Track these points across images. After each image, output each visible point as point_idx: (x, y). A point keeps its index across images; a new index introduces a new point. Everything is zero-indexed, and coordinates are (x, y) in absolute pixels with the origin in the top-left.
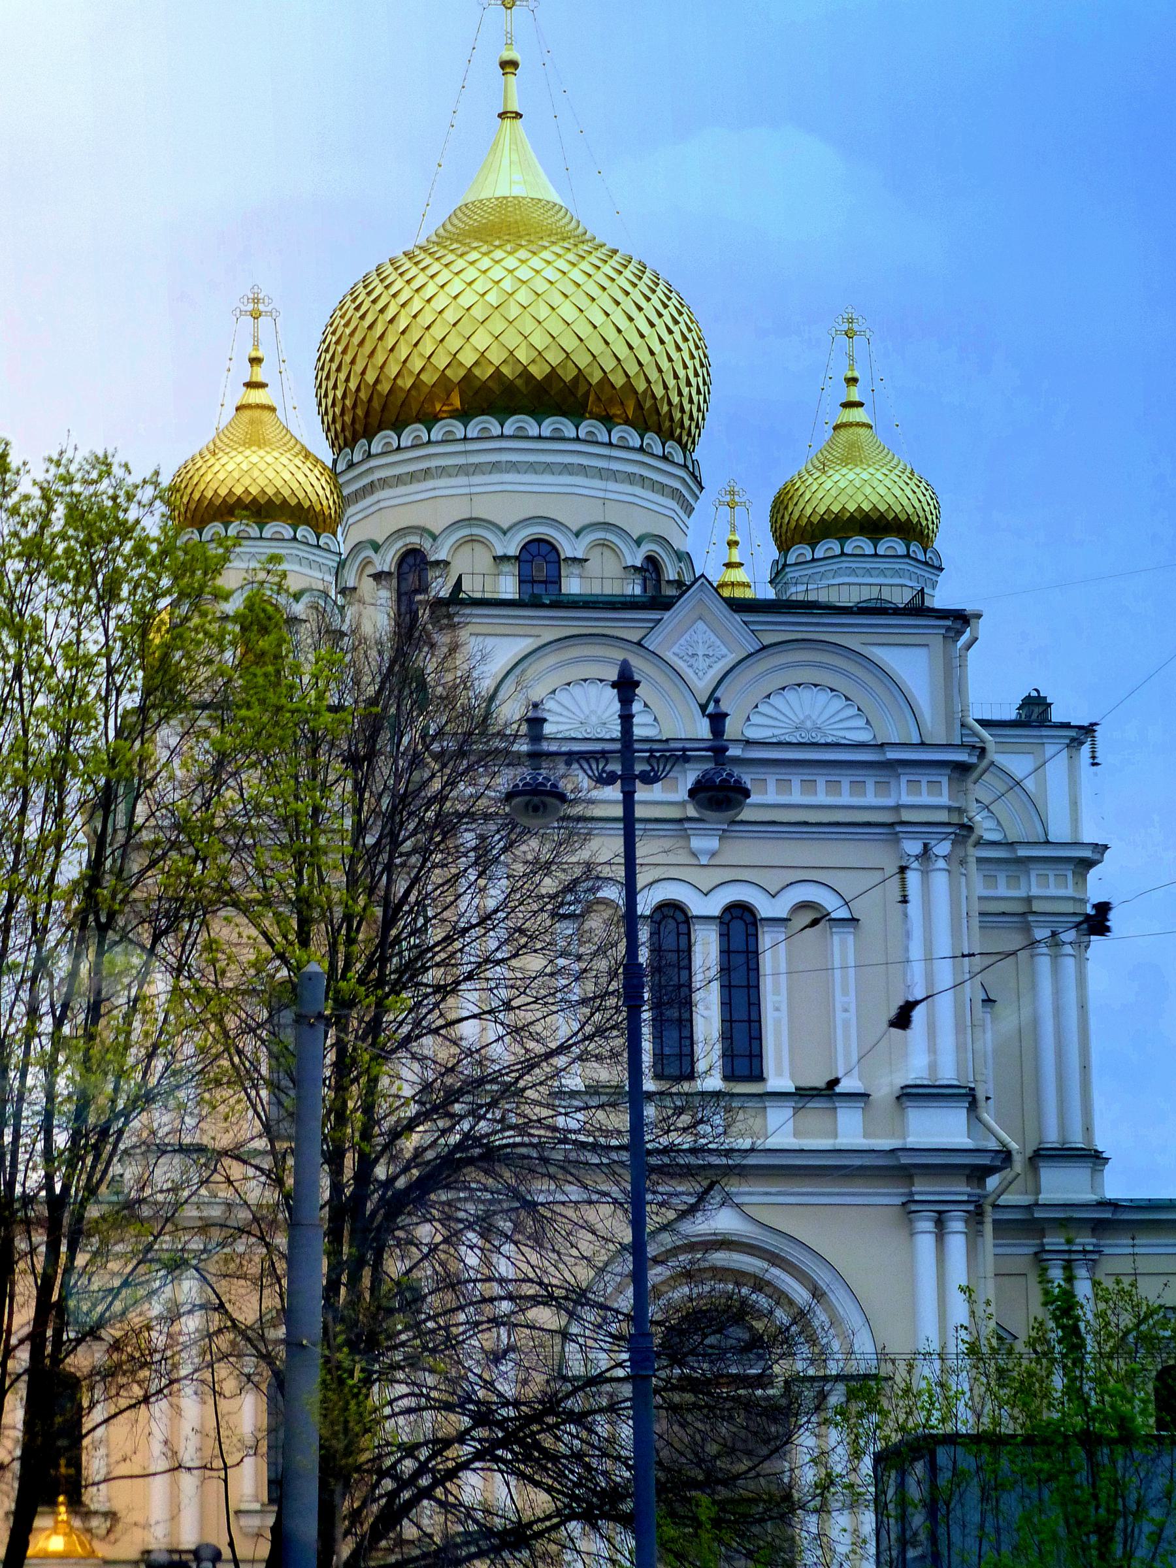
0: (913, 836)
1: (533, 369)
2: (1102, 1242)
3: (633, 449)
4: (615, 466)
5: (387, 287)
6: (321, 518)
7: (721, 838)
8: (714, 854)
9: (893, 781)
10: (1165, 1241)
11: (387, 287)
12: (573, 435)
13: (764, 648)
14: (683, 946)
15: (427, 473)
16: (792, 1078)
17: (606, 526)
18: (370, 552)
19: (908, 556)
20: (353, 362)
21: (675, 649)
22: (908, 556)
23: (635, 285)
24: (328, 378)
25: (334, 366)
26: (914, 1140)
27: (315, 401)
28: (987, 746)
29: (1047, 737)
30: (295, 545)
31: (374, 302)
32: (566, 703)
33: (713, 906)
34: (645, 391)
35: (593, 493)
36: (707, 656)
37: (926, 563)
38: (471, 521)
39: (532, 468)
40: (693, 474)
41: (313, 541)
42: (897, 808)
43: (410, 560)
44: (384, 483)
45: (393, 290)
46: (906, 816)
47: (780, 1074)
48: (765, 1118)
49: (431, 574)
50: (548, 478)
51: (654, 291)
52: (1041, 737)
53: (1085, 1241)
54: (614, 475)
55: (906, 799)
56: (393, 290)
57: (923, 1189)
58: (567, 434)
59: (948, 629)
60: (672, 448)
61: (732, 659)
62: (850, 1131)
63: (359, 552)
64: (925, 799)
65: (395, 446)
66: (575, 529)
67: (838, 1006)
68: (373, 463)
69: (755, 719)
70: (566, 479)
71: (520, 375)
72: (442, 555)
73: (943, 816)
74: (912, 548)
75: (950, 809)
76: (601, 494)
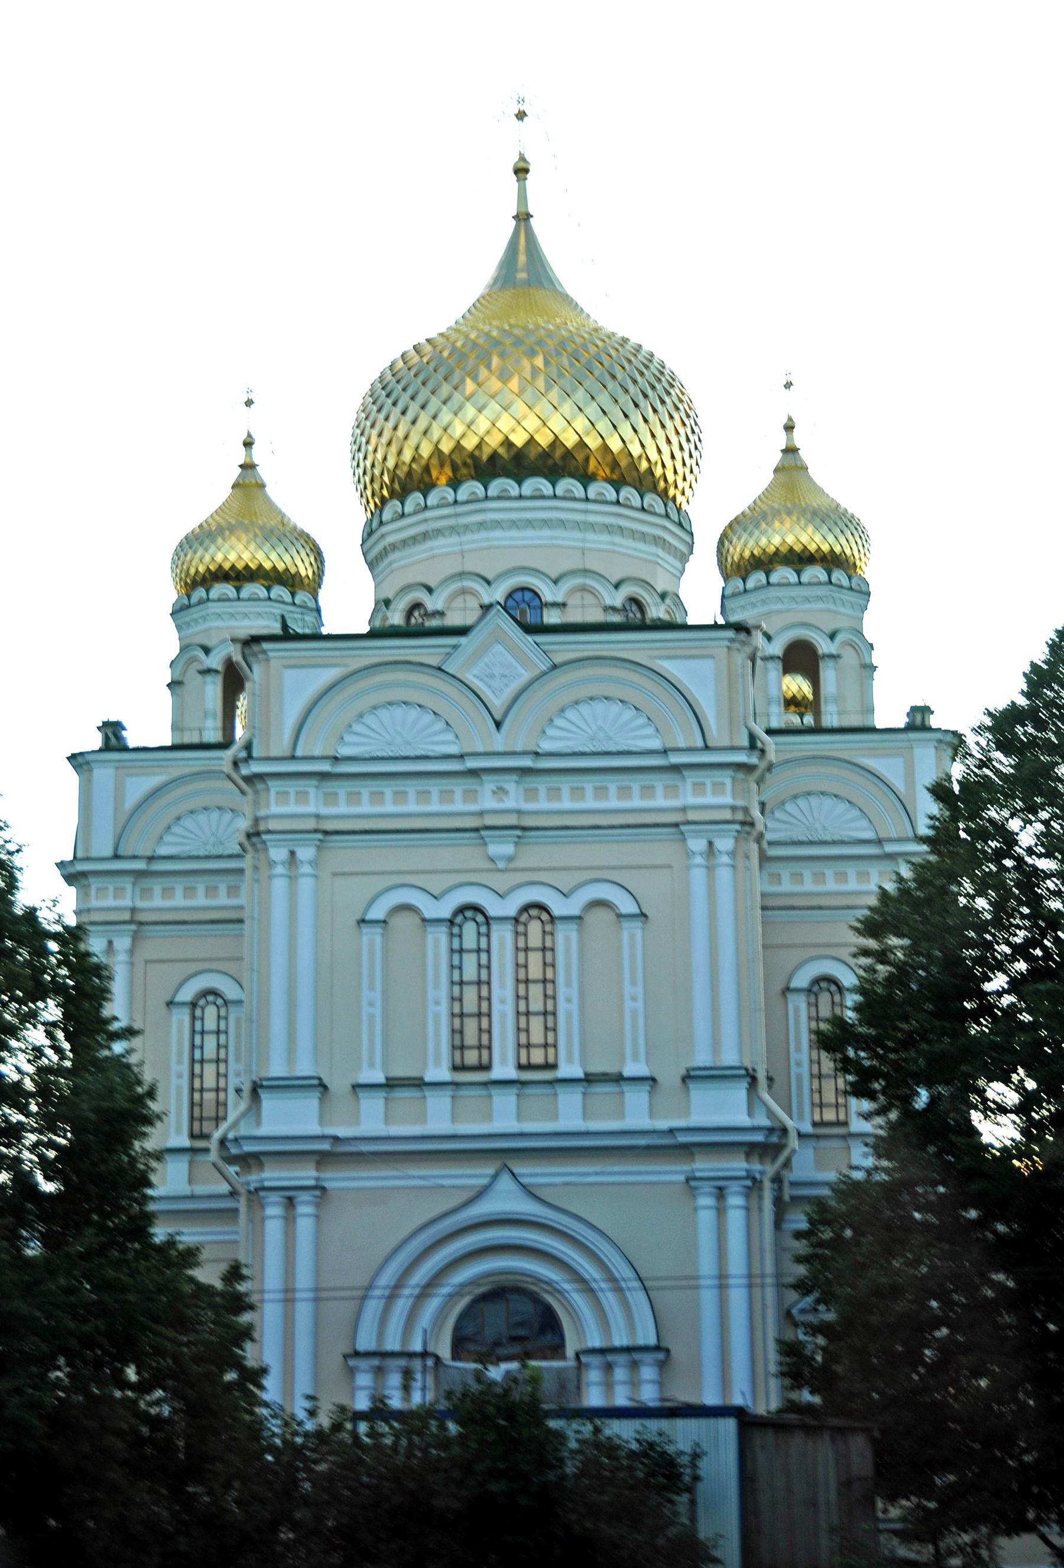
0: (697, 834)
1: (513, 438)
2: (323, 1175)
3: (611, 503)
4: (592, 518)
6: (297, 579)
7: (516, 844)
8: (510, 859)
9: (680, 784)
10: (365, 1174)
12: (582, 494)
13: (555, 667)
15: (425, 536)
16: (583, 1061)
17: (586, 572)
21: (475, 671)
26: (698, 1118)
28: (767, 749)
30: (269, 603)
32: (374, 726)
33: (510, 907)
34: (622, 451)
35: (572, 543)
36: (504, 676)
38: (461, 575)
39: (514, 524)
40: (680, 525)
42: (684, 809)
44: (394, 547)
46: (692, 816)
47: (570, 1060)
48: (556, 1100)
50: (530, 533)
51: (650, 361)
53: (306, 1174)
54: (592, 527)
55: (692, 800)
57: (704, 1165)
58: (577, 495)
59: (732, 640)
60: (651, 499)
61: (525, 676)
62: (636, 1113)
64: (710, 799)
66: (614, 579)
67: (627, 997)
69: (550, 732)
70: (546, 532)
71: (502, 444)
72: (439, 606)
73: (727, 815)
75: (734, 808)
76: (580, 544)
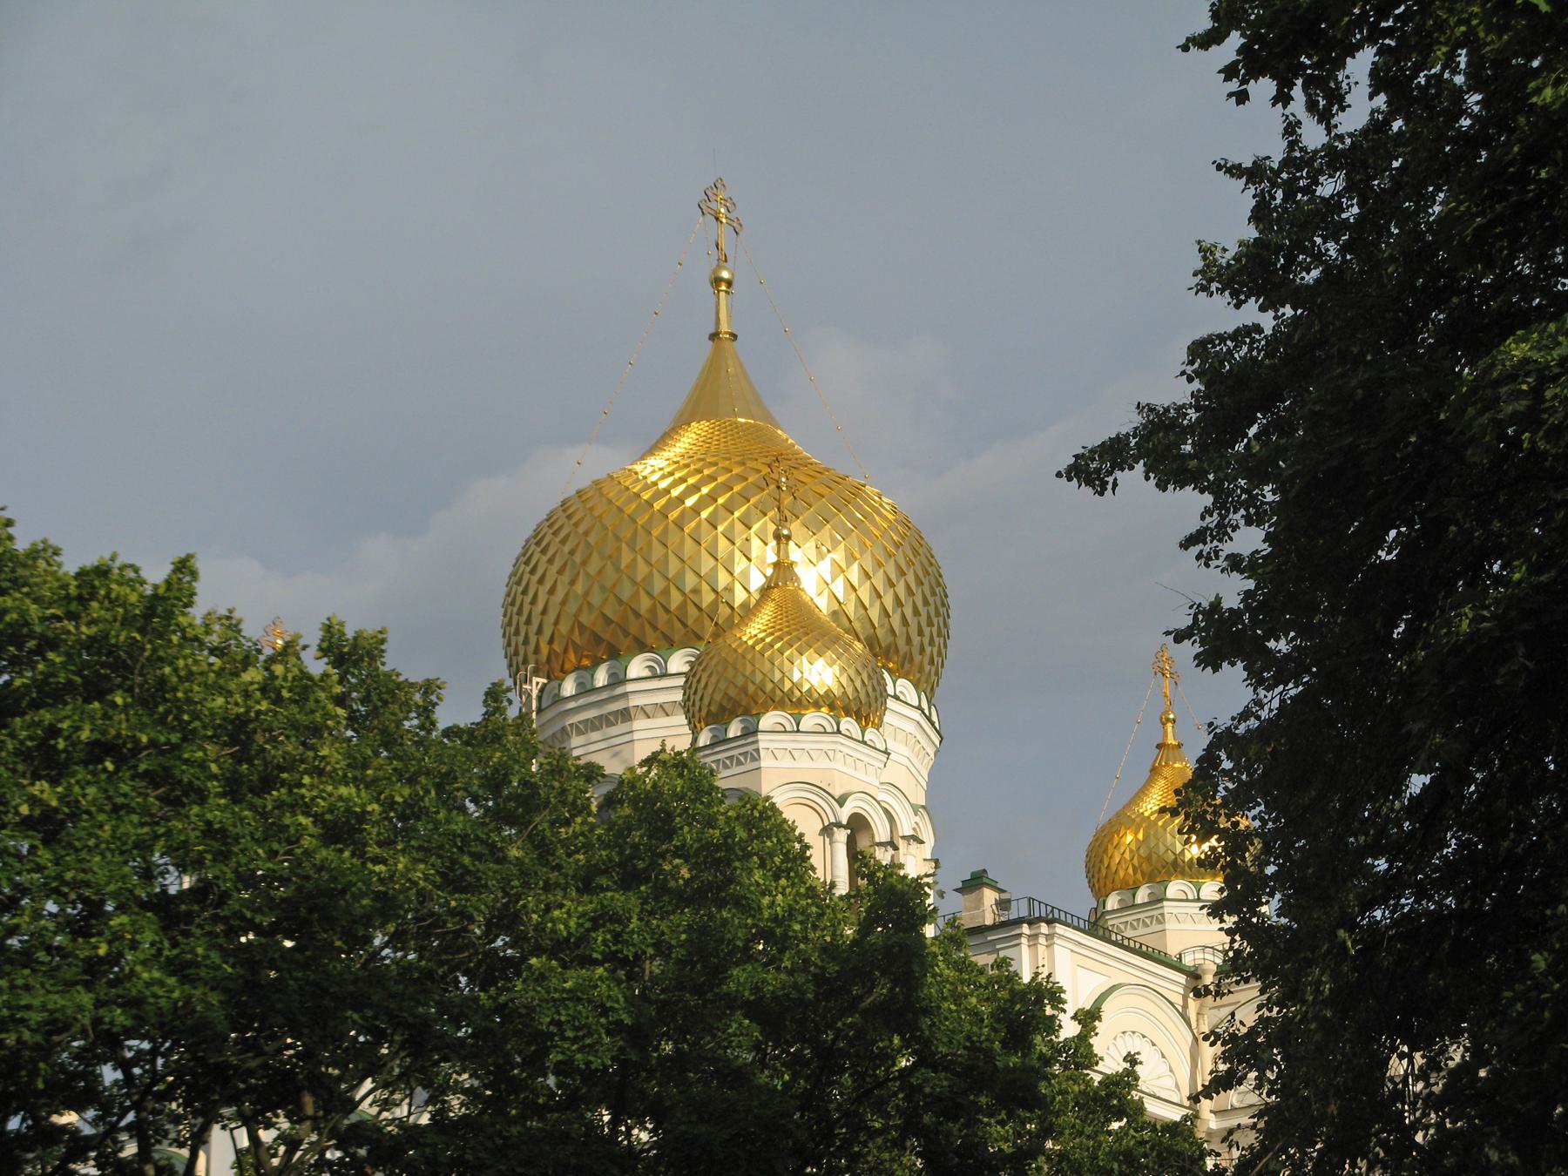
23: (892, 585)
30: (840, 739)
41: (857, 733)
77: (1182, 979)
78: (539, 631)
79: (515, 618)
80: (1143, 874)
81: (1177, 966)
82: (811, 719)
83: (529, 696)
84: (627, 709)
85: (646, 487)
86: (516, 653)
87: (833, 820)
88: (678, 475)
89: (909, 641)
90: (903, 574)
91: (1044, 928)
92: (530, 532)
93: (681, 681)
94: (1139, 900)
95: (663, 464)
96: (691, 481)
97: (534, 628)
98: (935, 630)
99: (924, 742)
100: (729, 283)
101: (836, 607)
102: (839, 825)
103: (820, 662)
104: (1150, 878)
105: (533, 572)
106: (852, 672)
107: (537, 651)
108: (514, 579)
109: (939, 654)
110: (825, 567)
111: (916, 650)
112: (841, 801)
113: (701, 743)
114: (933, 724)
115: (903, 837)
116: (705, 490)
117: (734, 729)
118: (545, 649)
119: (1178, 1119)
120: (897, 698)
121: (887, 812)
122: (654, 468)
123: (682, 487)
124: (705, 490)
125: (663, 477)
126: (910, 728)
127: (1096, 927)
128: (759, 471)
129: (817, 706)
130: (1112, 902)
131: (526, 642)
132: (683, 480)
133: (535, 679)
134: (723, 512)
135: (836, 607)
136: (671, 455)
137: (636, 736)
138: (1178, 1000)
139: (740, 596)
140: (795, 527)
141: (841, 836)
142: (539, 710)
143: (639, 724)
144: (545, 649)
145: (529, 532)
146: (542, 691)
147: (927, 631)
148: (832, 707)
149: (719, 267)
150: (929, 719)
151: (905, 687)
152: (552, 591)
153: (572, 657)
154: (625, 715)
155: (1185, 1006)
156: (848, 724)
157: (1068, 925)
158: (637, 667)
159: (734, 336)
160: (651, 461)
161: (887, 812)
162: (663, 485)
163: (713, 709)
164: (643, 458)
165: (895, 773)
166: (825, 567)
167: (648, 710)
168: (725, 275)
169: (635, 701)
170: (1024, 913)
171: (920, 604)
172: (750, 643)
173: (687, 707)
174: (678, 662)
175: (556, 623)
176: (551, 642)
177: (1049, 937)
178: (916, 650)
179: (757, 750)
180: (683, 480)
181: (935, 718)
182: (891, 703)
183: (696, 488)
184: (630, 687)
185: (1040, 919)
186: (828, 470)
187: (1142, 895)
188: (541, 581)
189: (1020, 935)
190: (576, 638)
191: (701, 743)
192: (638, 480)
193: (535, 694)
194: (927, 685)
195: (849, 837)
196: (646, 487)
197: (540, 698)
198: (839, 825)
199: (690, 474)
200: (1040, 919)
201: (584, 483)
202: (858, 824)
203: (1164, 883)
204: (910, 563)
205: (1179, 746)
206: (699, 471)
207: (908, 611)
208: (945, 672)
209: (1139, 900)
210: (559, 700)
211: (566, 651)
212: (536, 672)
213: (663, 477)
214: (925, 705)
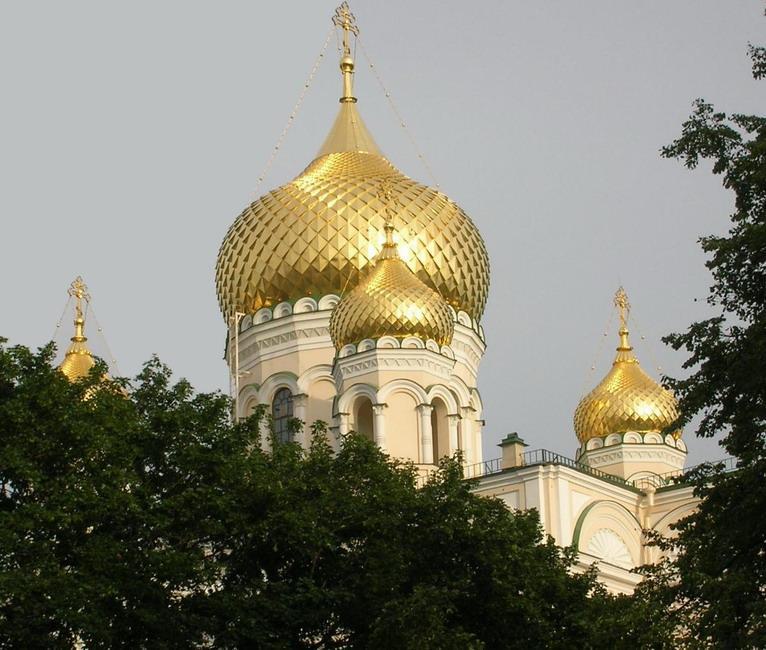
5: (261, 219)
11: (261, 219)
14: (278, 401)
18: (253, 392)
19: (665, 444)
20: (242, 272)
22: (665, 444)
23: (454, 235)
24: (225, 285)
25: (228, 289)
27: (218, 302)
29: (524, 476)
30: (426, 352)
31: (253, 229)
37: (676, 448)
41: (437, 350)
43: (281, 396)
45: (265, 220)
49: (296, 403)
52: (521, 477)
56: (265, 220)
63: (248, 391)
65: (270, 318)
68: (255, 330)
74: (666, 439)
77: (635, 496)
78: (239, 284)
79: (224, 276)
80: (609, 427)
81: (633, 489)
82: (409, 340)
83: (234, 323)
84: (294, 332)
85: (304, 195)
86: (225, 297)
87: (422, 402)
88: (323, 188)
89: (465, 288)
90: (454, 235)
91: (552, 468)
92: (232, 223)
93: (329, 314)
94: (607, 444)
95: (314, 181)
96: (331, 191)
97: (236, 282)
98: (481, 280)
99: (475, 348)
100: (352, 67)
101: (420, 268)
102: (426, 405)
103: (413, 307)
104: (614, 431)
105: (234, 248)
106: (433, 311)
107: (238, 296)
108: (223, 252)
109: (484, 283)
110: (414, 243)
111: (469, 293)
112: (428, 390)
113: (341, 356)
114: (480, 338)
115: (463, 408)
116: (339, 197)
117: (362, 347)
118: (243, 295)
119: (629, 592)
120: (458, 322)
121: (451, 390)
122: (307, 183)
123: (325, 196)
124: (339, 197)
125: (314, 189)
126: (467, 341)
127: (581, 465)
128: (373, 185)
129: (412, 332)
130: (590, 446)
131: (231, 290)
132: (326, 191)
133: (237, 314)
134: (351, 211)
135: (420, 268)
136: (318, 175)
137: (299, 348)
138: (632, 509)
139: (362, 263)
140: (395, 222)
141: (428, 411)
142: (240, 333)
143: (301, 341)
144: (243, 295)
145: (232, 222)
146: (241, 321)
147: (476, 281)
148: (421, 333)
149: (345, 57)
150: (478, 335)
151: (463, 316)
152: (246, 260)
153: (260, 300)
154: (293, 335)
155: (637, 513)
156: (431, 343)
157: (566, 466)
158: (300, 306)
159: (355, 100)
160: (306, 178)
161: (451, 390)
162: (313, 194)
163: (349, 335)
164: (301, 175)
165: (459, 370)
166: (414, 243)
167: (306, 332)
168: (349, 61)
169: (298, 327)
170: (540, 459)
171: (472, 265)
172: (371, 294)
173: (331, 330)
174: (325, 303)
175: (250, 279)
176: (246, 291)
177: (556, 473)
178: (469, 293)
179: (376, 360)
180: (326, 191)
181: (481, 335)
182: (457, 327)
183: (335, 195)
184: (295, 319)
185: (549, 463)
186: (415, 183)
187: (609, 441)
188: (240, 253)
189: (538, 473)
190: (262, 288)
191: (341, 356)
192: (298, 192)
193: (237, 322)
194: (476, 314)
195: (432, 412)
196: (304, 195)
197: (240, 325)
198: (426, 405)
199: (329, 188)
200: (549, 463)
201: (265, 192)
202: (437, 403)
203: (622, 435)
204: (462, 223)
205: (630, 349)
206: (336, 185)
207: (465, 269)
208: (486, 306)
209: (607, 444)
210: (252, 326)
211: (255, 296)
212: (238, 309)
213: (314, 189)
214: (475, 327)
